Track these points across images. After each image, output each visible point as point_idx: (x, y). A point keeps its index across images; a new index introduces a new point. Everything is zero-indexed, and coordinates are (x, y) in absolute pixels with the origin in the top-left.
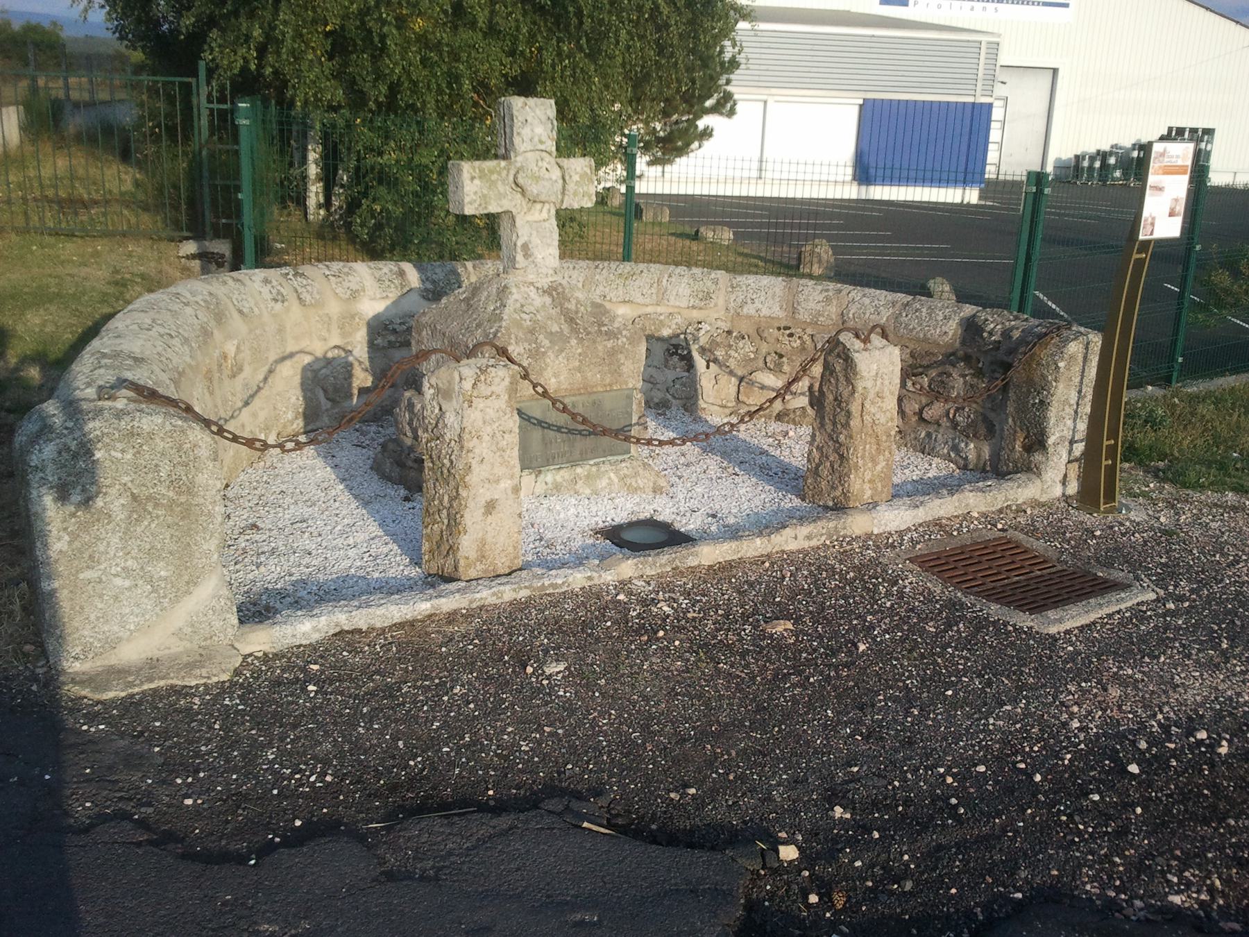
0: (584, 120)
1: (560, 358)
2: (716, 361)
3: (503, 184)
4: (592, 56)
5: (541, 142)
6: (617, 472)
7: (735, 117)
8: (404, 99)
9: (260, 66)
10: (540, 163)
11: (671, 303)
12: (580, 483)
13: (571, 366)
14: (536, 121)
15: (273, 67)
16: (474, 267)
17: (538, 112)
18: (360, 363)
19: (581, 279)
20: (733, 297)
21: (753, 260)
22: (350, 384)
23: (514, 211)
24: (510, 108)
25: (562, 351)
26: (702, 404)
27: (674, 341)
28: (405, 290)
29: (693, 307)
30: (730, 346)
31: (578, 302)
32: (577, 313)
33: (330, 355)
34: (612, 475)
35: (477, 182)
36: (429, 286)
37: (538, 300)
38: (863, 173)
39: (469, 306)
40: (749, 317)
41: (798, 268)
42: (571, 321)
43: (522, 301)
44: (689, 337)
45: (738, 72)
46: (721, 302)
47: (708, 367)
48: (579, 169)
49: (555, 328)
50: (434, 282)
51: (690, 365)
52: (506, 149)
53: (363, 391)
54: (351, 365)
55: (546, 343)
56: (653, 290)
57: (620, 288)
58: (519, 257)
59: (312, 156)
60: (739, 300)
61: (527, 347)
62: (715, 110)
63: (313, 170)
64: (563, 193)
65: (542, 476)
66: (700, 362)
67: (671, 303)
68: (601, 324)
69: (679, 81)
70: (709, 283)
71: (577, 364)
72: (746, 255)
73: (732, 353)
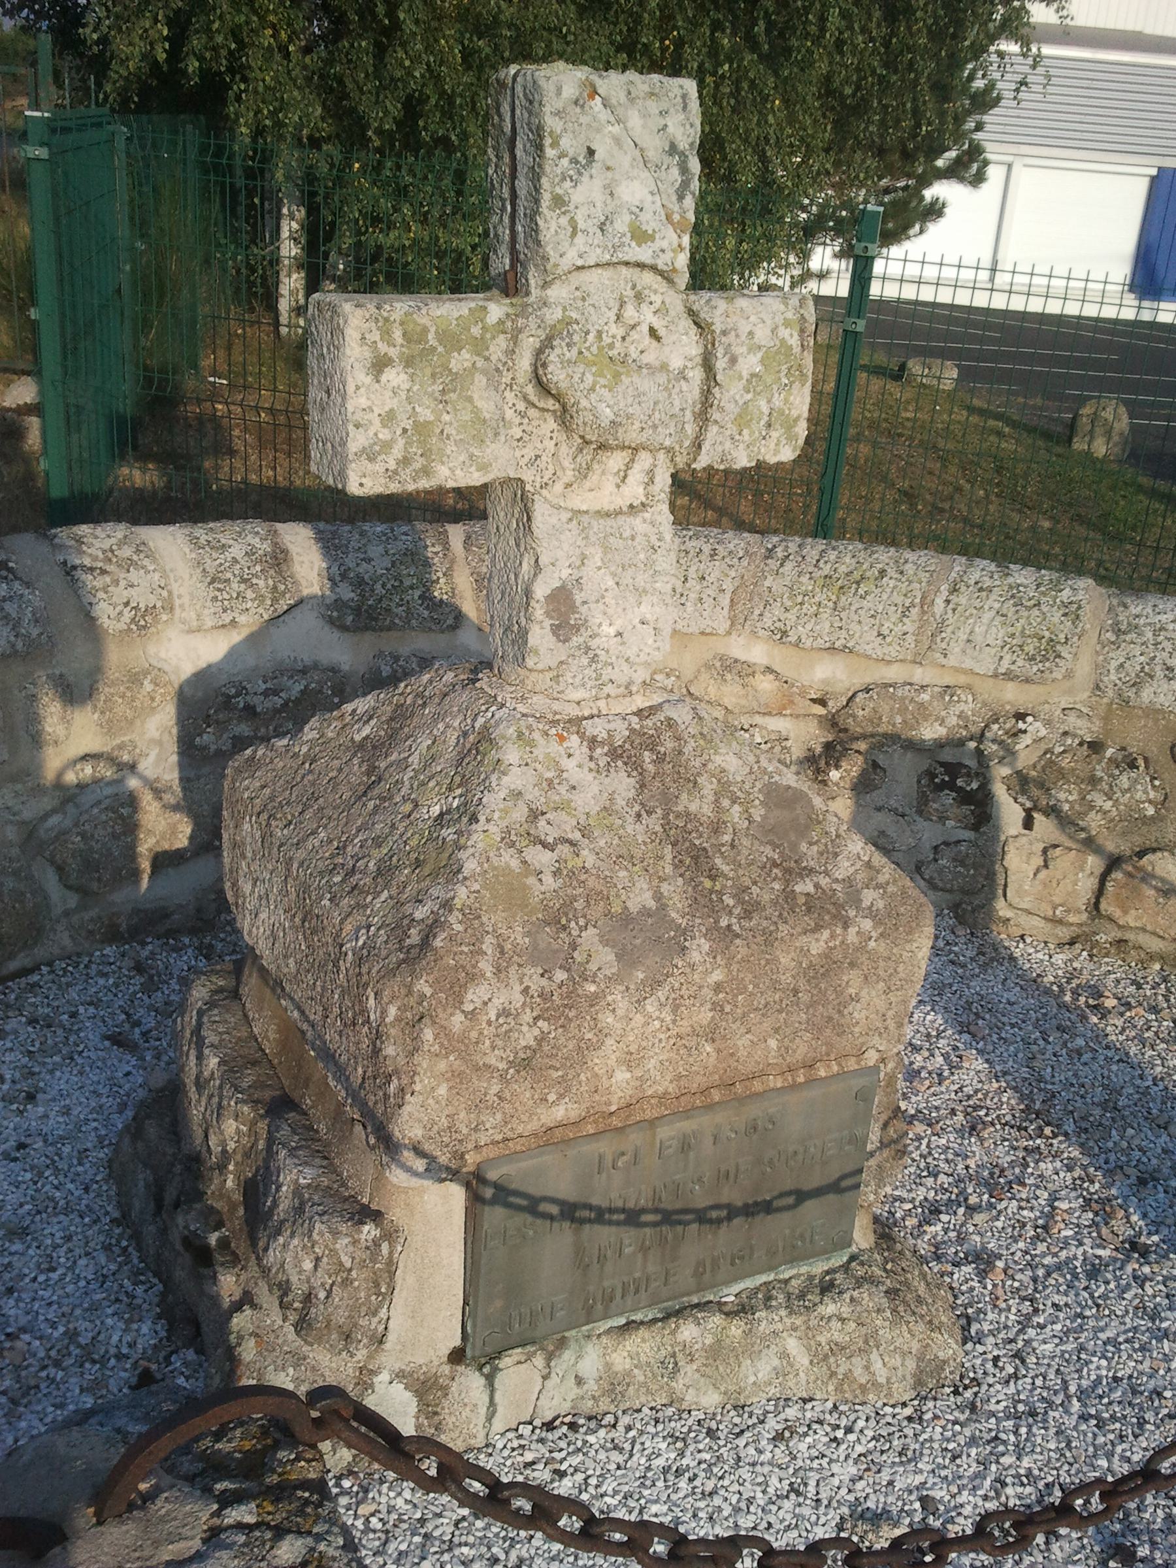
0: (747, 180)
1: (650, 1007)
2: (1053, 811)
3: (494, 384)
4: (771, 60)
5: (641, 236)
6: (807, 1335)
7: (984, 186)
8: (430, 126)
9: (175, 54)
10: (630, 312)
11: (952, 661)
12: (689, 1371)
13: (684, 1026)
14: (625, 159)
15: (201, 59)
16: (468, 542)
17: (635, 120)
18: (157, 793)
19: (728, 586)
20: (1118, 657)
21: (991, 423)
22: (131, 854)
23: (528, 476)
24: (533, 101)
25: (656, 984)
26: (1001, 909)
27: (948, 756)
28: (283, 606)
29: (1009, 676)
30: (1093, 781)
31: (724, 787)
32: (717, 828)
33: (70, 778)
34: (792, 1345)
35: (394, 376)
36: (347, 593)
37: (593, 788)
38: (1147, 278)
39: (375, 777)
40: (1153, 712)
41: (1070, 441)
42: (696, 861)
43: (533, 795)
44: (991, 748)
45: (996, 111)
46: (1084, 669)
47: (1028, 824)
48: (762, 335)
49: (640, 897)
50: (359, 583)
51: (981, 809)
52: (514, 252)
53: (164, 861)
54: (132, 801)
55: (605, 959)
56: (909, 626)
57: (826, 613)
58: (540, 636)
59: (289, 227)
60: (1133, 668)
61: (536, 983)
62: (954, 172)
63: (289, 250)
64: (703, 415)
65: (568, 1355)
66: (1009, 811)
67: (952, 661)
68: (794, 870)
69: (916, 113)
70: (1056, 616)
71: (705, 1016)
72: (981, 412)
73: (1099, 799)
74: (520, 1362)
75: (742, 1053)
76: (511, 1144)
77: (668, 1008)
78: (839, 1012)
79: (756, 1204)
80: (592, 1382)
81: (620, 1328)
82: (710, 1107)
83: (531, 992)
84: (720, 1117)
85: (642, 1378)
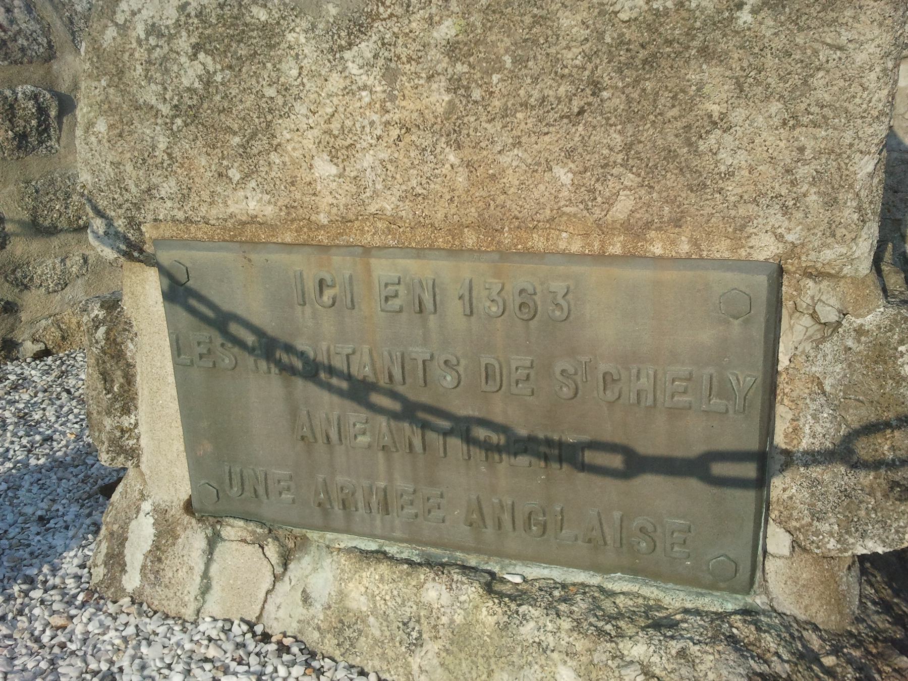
71: (438, 98)
74: (244, 541)
75: (511, 179)
76: (192, 229)
77: (376, 71)
78: (689, 143)
79: (549, 442)
80: (319, 606)
81: (362, 551)
82: (455, 253)
83: (189, 9)
84: (467, 269)
85: (377, 633)
